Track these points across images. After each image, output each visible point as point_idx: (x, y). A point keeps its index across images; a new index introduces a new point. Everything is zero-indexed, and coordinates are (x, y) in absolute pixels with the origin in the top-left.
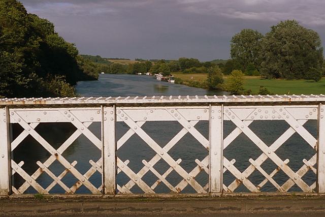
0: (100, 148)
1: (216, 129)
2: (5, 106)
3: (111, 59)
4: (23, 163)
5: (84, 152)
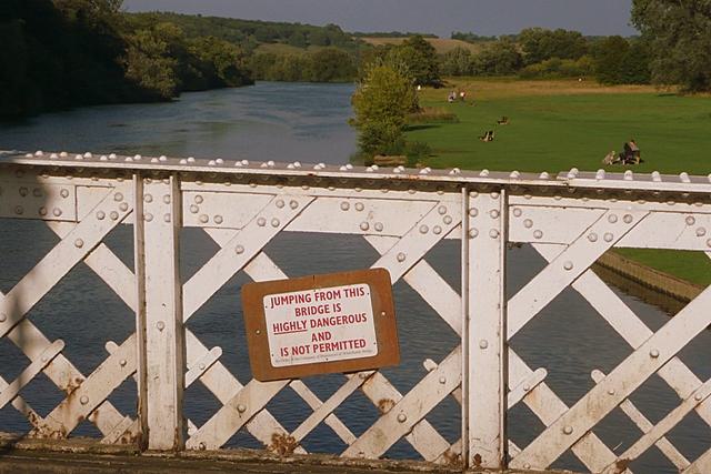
0: (132, 301)
1: (484, 263)
2: (170, 173)
3: (370, 36)
4: (598, 371)
5: (412, 335)
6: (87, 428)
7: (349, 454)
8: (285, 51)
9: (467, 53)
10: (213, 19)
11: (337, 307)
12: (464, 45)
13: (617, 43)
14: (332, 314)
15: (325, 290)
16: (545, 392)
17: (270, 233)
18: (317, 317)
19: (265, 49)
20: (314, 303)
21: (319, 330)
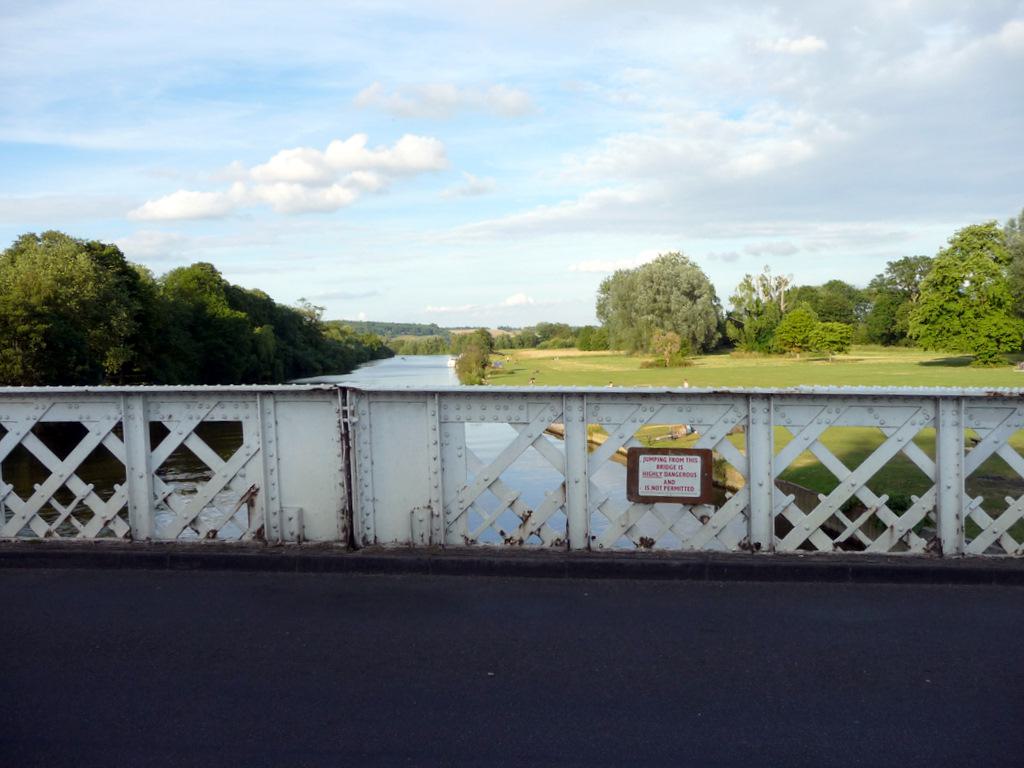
5: (104, 471)
6: (807, 545)
7: (79, 537)
8: (410, 339)
9: (508, 336)
10: (368, 322)
11: (681, 467)
12: (506, 333)
13: (589, 330)
14: (677, 470)
15: (675, 457)
16: (795, 509)
17: (196, 423)
18: (669, 471)
19: (399, 338)
20: (668, 463)
21: (671, 478)
